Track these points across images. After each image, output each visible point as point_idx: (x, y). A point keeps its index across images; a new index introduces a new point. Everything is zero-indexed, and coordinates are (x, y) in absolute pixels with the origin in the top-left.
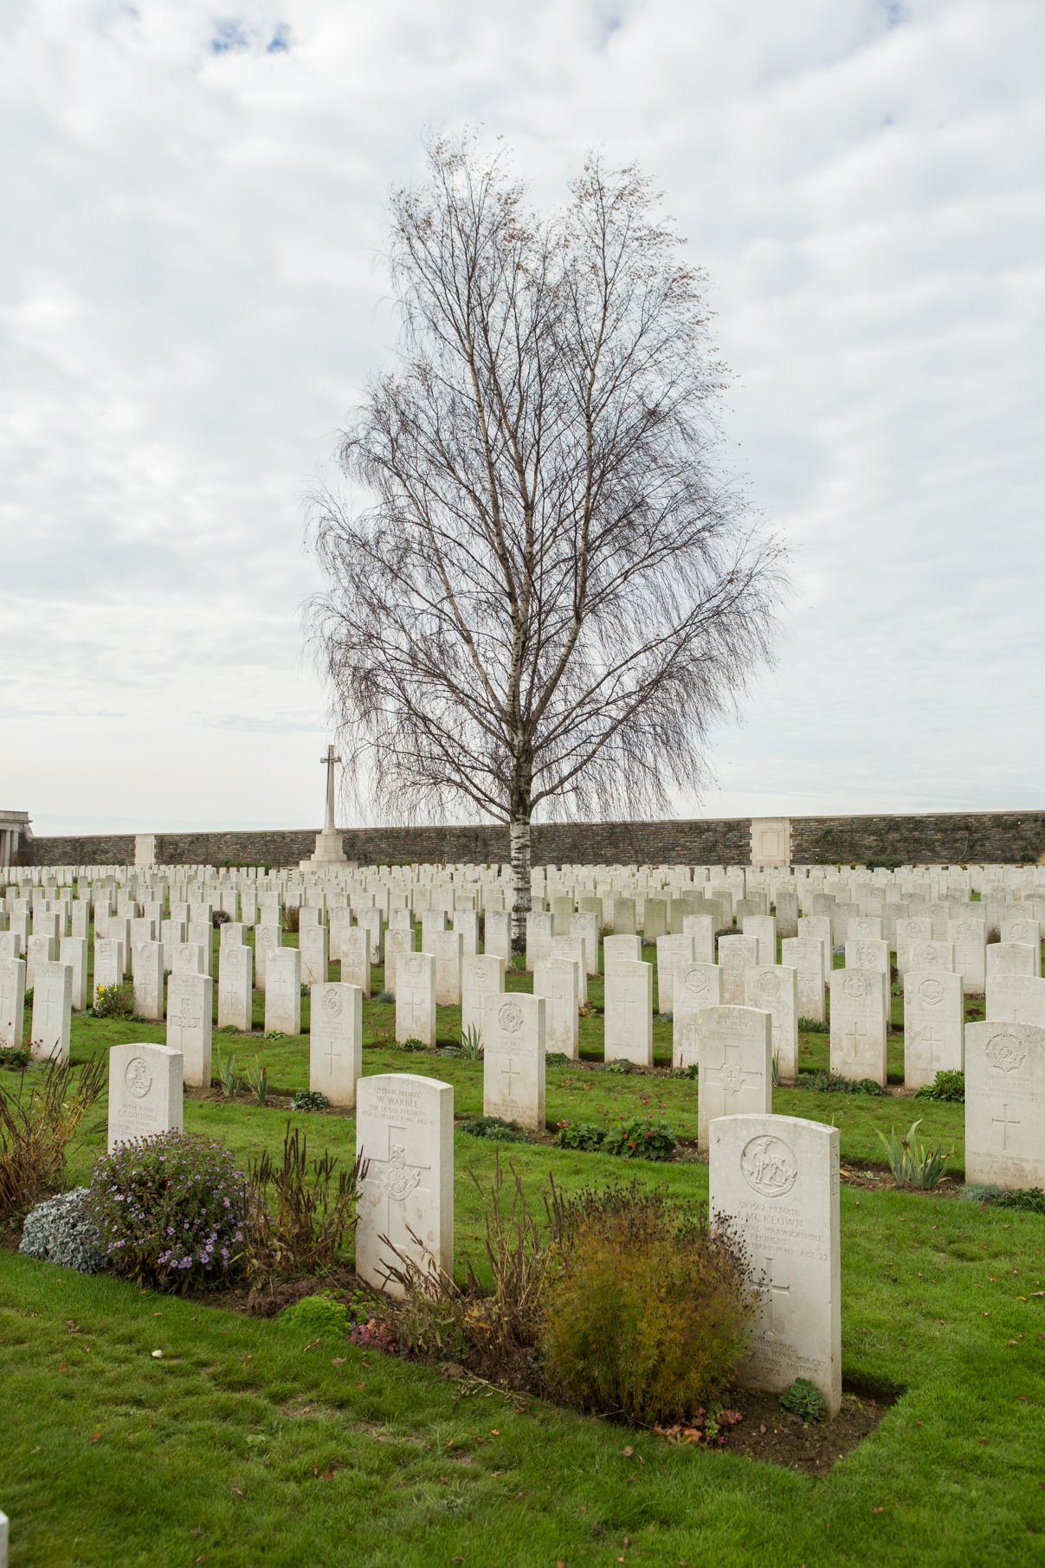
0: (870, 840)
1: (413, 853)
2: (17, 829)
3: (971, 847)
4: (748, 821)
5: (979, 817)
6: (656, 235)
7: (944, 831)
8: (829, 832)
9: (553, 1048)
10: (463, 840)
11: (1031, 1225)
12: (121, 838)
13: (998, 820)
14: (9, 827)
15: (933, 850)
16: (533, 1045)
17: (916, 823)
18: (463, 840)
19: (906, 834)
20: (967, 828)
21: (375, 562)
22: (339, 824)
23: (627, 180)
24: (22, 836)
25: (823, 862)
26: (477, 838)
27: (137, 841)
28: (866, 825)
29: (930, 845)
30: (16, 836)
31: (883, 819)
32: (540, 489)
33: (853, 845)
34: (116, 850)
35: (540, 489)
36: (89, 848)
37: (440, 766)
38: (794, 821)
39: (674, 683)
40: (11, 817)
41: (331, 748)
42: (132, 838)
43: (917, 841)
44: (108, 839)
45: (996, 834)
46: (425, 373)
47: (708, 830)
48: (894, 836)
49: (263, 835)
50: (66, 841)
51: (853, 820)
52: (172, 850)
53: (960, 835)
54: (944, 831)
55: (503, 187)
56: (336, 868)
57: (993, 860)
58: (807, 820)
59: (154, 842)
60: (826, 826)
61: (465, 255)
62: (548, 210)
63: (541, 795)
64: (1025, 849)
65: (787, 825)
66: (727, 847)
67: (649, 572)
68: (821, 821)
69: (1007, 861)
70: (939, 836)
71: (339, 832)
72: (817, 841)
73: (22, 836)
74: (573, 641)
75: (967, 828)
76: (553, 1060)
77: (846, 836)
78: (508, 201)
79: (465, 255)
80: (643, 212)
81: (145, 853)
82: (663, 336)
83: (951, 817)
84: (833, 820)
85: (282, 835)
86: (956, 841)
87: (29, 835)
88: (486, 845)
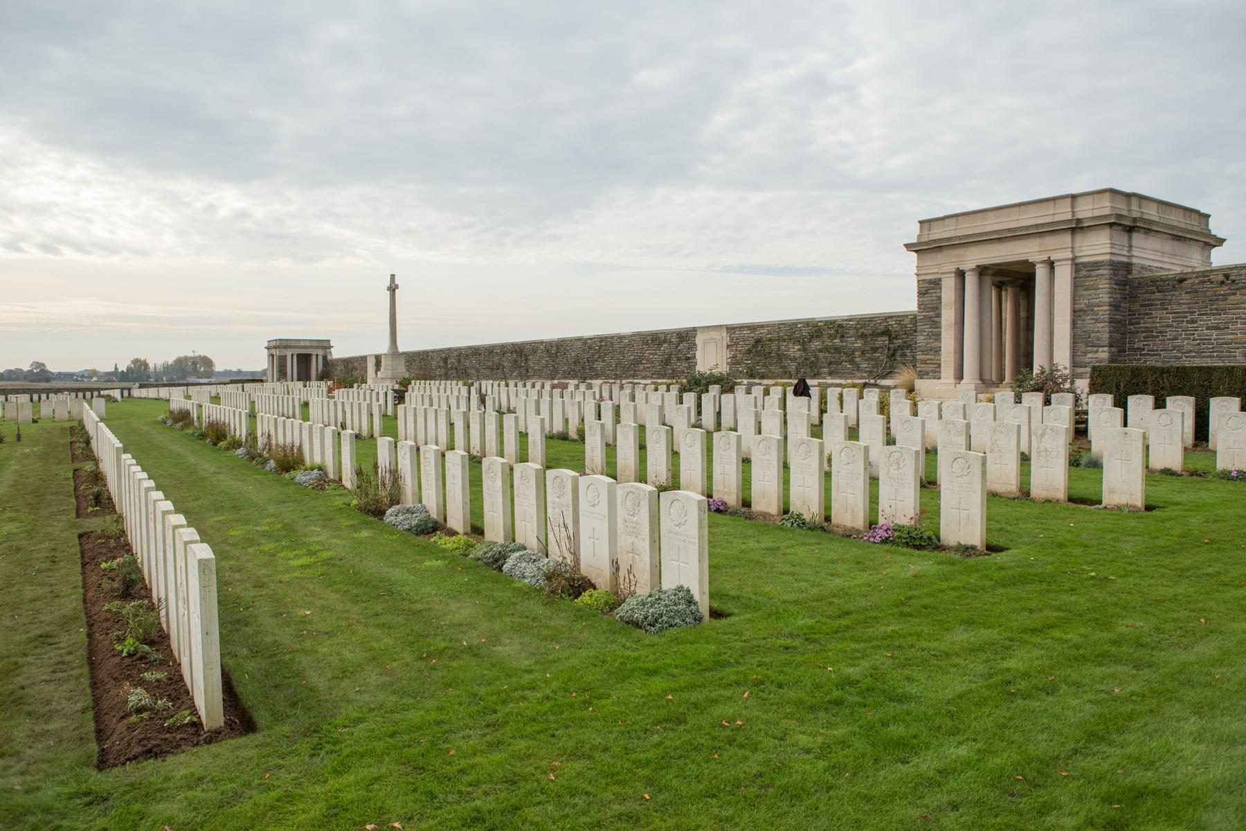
2: (321, 353)
4: (695, 329)
7: (863, 336)
8: (758, 341)
9: (1157, 462)
14: (314, 352)
15: (852, 361)
16: (977, 486)
19: (828, 342)
22: (402, 348)
24: (325, 358)
27: (699, 340)
30: (320, 359)
38: (731, 329)
40: (315, 344)
41: (393, 276)
43: (837, 350)
47: (665, 342)
48: (816, 344)
54: (863, 336)
58: (741, 327)
60: (756, 335)
66: (679, 359)
68: (752, 328)
70: (858, 344)
72: (749, 351)
73: (325, 358)
75: (886, 332)
76: (992, 497)
84: (762, 326)
85: (621, 338)
86: (875, 350)
87: (329, 357)
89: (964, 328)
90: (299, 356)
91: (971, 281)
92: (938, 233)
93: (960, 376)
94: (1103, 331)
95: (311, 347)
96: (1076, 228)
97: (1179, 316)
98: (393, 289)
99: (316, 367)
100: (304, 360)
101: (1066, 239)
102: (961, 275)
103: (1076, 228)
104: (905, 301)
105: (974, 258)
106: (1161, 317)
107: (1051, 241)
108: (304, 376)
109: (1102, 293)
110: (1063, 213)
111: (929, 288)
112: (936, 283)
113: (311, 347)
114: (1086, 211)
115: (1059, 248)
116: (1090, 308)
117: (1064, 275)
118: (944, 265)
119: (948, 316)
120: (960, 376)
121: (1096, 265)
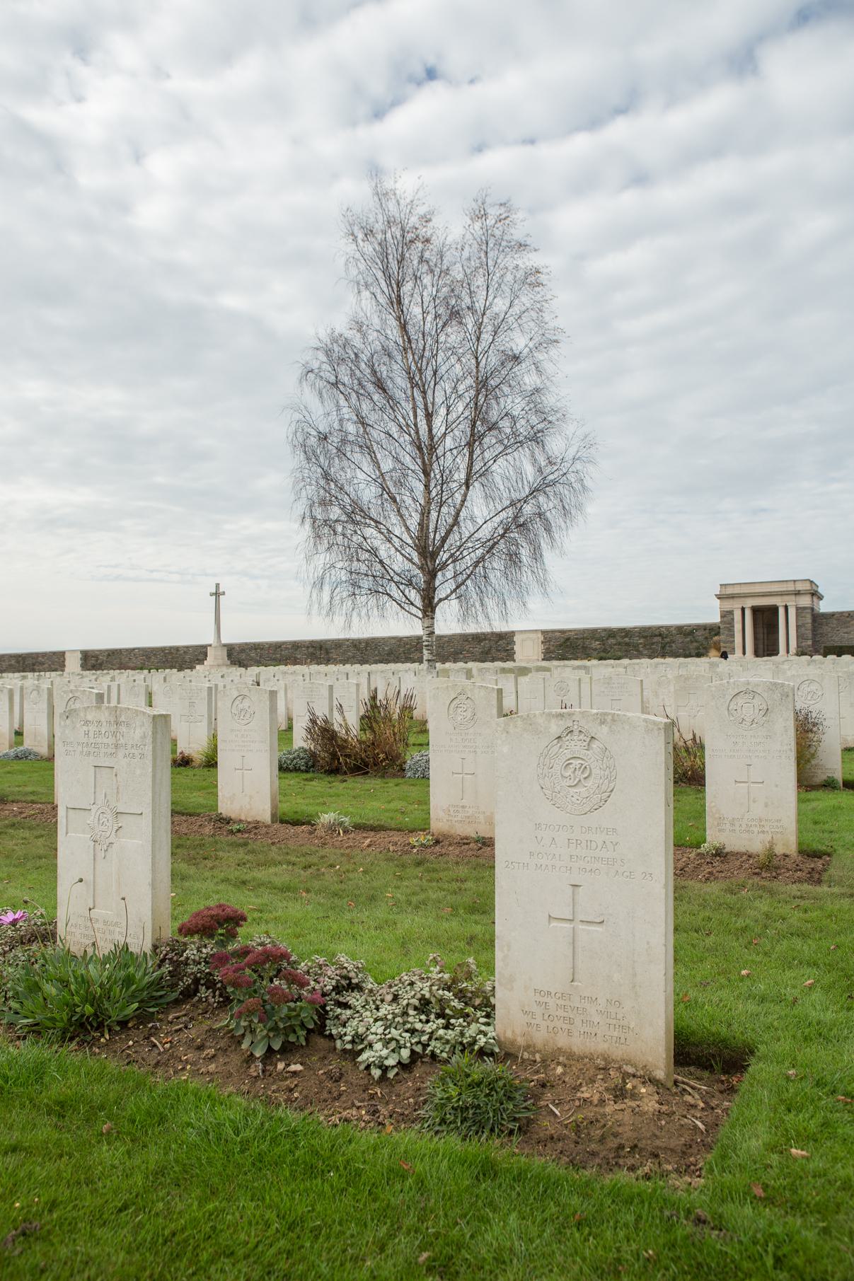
0: (596, 644)
1: (275, 659)
3: (663, 648)
5: (668, 628)
6: (522, 246)
7: (645, 637)
8: (568, 639)
10: (311, 650)
11: (846, 798)
12: (54, 653)
13: (680, 629)
17: (626, 632)
18: (311, 650)
19: (620, 640)
20: (660, 635)
21: (322, 451)
23: (503, 210)
25: (564, 658)
26: (321, 648)
27: (67, 655)
28: (593, 634)
29: (636, 647)
31: (605, 630)
32: (428, 406)
33: (585, 648)
34: (51, 662)
35: (428, 406)
36: (29, 661)
37: (370, 579)
38: (543, 632)
39: (521, 531)
41: (218, 586)
42: (63, 653)
43: (628, 644)
44: (44, 655)
45: (679, 639)
46: (360, 327)
49: (163, 649)
50: (11, 656)
51: (584, 631)
52: (93, 661)
53: (656, 639)
54: (645, 637)
55: (421, 210)
56: (224, 670)
57: (676, 655)
58: (553, 631)
59: (80, 656)
61: (395, 254)
62: (452, 229)
63: (441, 600)
64: (698, 648)
65: (540, 635)
67: (509, 457)
69: (686, 656)
71: (225, 645)
74: (463, 501)
75: (660, 635)
77: (580, 642)
78: (426, 219)
79: (395, 254)
80: (512, 231)
81: (73, 664)
82: (524, 308)
83: (650, 628)
85: (177, 649)
88: (327, 653)
89: (743, 632)
90: (756, 611)
91: (748, 614)
92: (729, 591)
93: (744, 653)
94: (809, 634)
95: (781, 594)
96: (798, 593)
97: (833, 629)
98: (217, 594)
99: (788, 632)
100: (766, 619)
101: (793, 597)
102: (743, 610)
103: (798, 593)
104: (715, 619)
105: (750, 603)
106: (826, 629)
107: (786, 598)
108: (766, 645)
109: (809, 619)
110: (791, 587)
111: (727, 615)
112: (731, 613)
113: (781, 594)
114: (800, 587)
115: (792, 602)
116: (803, 625)
117: (792, 612)
118: (736, 606)
119: (738, 627)
120: (744, 653)
121: (805, 608)
